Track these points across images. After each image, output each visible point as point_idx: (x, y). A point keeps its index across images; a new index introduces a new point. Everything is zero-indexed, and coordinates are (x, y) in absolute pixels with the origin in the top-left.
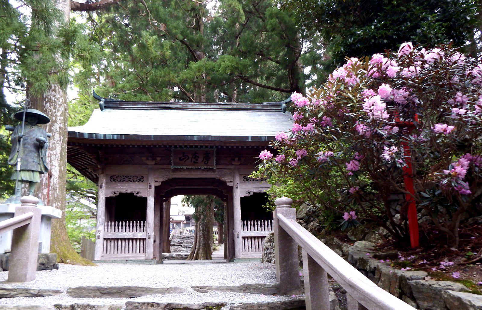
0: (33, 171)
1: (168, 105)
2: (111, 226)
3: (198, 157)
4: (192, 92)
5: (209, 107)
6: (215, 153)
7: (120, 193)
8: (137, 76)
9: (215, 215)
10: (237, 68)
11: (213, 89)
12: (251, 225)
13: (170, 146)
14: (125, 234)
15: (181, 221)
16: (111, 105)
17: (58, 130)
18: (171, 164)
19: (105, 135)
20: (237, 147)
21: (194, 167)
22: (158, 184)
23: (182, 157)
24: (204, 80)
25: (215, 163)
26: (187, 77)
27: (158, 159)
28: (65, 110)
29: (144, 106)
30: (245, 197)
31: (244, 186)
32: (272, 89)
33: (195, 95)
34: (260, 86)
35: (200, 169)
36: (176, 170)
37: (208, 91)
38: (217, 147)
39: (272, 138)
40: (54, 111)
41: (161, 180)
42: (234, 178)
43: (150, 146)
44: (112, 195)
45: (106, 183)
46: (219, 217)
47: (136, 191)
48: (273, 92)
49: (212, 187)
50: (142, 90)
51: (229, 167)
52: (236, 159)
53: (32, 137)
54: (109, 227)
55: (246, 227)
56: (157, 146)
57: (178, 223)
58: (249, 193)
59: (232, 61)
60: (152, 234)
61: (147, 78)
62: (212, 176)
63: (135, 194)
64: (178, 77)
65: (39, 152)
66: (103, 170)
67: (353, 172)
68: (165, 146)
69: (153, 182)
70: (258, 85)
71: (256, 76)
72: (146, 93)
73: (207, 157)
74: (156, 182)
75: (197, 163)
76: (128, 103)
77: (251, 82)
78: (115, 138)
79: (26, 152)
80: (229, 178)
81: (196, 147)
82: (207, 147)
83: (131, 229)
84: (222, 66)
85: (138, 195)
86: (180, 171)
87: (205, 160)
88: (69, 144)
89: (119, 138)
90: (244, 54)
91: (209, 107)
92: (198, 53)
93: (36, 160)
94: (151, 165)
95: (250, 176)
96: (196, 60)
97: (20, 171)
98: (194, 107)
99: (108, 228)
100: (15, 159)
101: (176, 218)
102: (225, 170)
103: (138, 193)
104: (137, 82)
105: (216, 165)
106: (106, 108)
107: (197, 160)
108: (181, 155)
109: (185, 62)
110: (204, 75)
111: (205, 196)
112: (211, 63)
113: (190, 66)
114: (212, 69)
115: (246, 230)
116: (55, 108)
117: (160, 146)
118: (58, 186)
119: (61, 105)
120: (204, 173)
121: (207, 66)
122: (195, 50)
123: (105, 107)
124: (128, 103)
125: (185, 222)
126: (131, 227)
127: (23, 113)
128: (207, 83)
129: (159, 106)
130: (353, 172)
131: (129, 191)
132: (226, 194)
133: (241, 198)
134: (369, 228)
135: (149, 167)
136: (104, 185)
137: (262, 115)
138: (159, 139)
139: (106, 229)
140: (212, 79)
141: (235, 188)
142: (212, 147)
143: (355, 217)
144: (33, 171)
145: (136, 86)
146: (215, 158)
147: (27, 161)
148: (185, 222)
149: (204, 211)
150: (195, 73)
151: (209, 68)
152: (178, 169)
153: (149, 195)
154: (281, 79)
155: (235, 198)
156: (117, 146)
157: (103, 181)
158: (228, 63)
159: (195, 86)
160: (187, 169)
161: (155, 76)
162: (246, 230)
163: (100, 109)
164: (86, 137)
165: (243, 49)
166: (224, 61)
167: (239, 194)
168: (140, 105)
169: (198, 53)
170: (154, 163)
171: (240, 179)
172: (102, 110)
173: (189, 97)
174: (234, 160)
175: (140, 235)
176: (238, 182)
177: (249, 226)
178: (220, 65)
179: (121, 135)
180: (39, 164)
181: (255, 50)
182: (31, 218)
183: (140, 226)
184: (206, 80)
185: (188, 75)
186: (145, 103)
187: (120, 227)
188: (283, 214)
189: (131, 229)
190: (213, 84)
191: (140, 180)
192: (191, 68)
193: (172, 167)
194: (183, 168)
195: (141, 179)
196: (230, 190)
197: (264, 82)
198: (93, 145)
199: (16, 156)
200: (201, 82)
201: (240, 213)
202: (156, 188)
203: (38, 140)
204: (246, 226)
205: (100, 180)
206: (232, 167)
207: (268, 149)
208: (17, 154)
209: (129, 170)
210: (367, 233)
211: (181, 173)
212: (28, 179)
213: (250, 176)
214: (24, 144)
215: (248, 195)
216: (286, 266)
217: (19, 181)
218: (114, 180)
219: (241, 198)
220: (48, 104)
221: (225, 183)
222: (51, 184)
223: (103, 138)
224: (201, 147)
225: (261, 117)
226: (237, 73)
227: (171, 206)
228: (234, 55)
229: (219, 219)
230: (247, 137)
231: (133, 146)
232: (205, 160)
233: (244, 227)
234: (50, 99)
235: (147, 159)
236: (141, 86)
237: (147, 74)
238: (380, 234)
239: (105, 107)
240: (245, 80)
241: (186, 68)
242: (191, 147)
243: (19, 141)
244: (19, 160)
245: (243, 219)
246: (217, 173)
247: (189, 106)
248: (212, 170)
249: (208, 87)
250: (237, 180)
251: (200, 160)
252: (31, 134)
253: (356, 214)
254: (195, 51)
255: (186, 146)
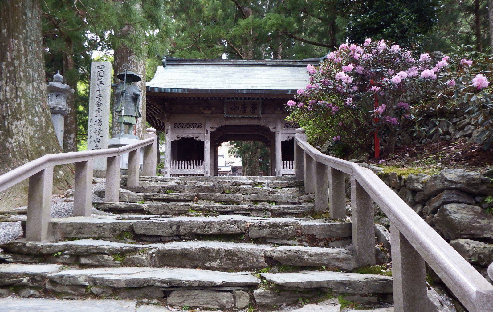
0: (132, 116)
1: (221, 62)
2: (176, 164)
3: (247, 107)
4: (240, 47)
5: (256, 63)
6: (260, 104)
7: (182, 138)
8: (190, 34)
9: (261, 163)
10: (281, 26)
11: (260, 44)
12: (290, 164)
13: (224, 98)
14: (187, 170)
15: (227, 172)
16: (172, 63)
17: (140, 86)
18: (224, 114)
19: (171, 89)
20: (279, 99)
21: (243, 116)
22: (213, 130)
23: (234, 108)
24: (251, 37)
25: (260, 113)
26: (236, 34)
27: (214, 109)
28: (144, 69)
29: (200, 63)
30: (286, 141)
31: (284, 132)
32: (315, 44)
33: (243, 49)
34: (305, 42)
35: (248, 117)
36: (228, 118)
37: (255, 46)
38: (262, 98)
39: (295, 92)
40: (136, 70)
41: (216, 127)
42: (276, 125)
43: (208, 98)
44: (176, 139)
45: (171, 129)
46: (264, 166)
47: (196, 135)
48: (316, 47)
49: (257, 133)
50: (195, 47)
51: (272, 116)
52: (279, 109)
53: (130, 92)
54: (174, 165)
55: (285, 167)
56: (213, 98)
57: (225, 173)
58: (289, 138)
59: (278, 19)
60: (209, 171)
61: (200, 36)
62: (258, 124)
63: (195, 138)
64: (227, 34)
65: (135, 103)
66: (169, 118)
67: (336, 112)
68: (220, 98)
69: (210, 128)
70: (302, 40)
71: (300, 31)
72: (198, 50)
73: (254, 107)
74: (212, 128)
75: (246, 112)
76: (185, 60)
77: (295, 38)
78: (180, 92)
79: (127, 103)
80: (272, 126)
81: (245, 98)
82: (254, 99)
83: (192, 167)
84: (269, 23)
85: (198, 139)
86: (232, 119)
87: (252, 110)
88: (147, 97)
89: (183, 92)
90: (288, 12)
91: (256, 63)
92: (246, 9)
93: (133, 108)
94: (207, 114)
95: (285, 120)
96: (244, 17)
97: (125, 116)
98: (243, 63)
99: (173, 166)
100: (120, 107)
101: (223, 169)
102: (269, 119)
103: (197, 138)
104: (191, 40)
105: (262, 114)
106: (168, 65)
107: (246, 110)
108: (233, 106)
109: (233, 17)
110: (251, 31)
111: (252, 142)
112: (258, 21)
113: (238, 23)
114: (259, 27)
115: (285, 169)
116: (137, 69)
117: (216, 98)
118: (141, 129)
119: (141, 66)
120: (252, 121)
121: (254, 23)
122: (243, 6)
123: (167, 64)
124: (185, 60)
125: (231, 173)
126: (192, 165)
127: (124, 74)
128: (254, 39)
129: (213, 63)
130: (336, 112)
131: (190, 136)
132: (268, 139)
133: (282, 142)
134: (360, 152)
135: (206, 115)
136: (169, 131)
137: (302, 70)
138: (214, 92)
139: (172, 167)
140: (259, 35)
141: (277, 133)
142: (258, 99)
143: (339, 139)
144: (132, 116)
145: (191, 44)
146: (261, 108)
147: (128, 109)
148: (231, 173)
149: (250, 156)
150: (243, 30)
151: (256, 25)
152: (230, 117)
153: (206, 139)
154: (323, 35)
155: (277, 142)
156: (181, 98)
157: (168, 127)
158: (274, 21)
159: (242, 42)
160: (237, 117)
161: (207, 33)
162: (285, 169)
163: (162, 66)
164: (157, 90)
165: (288, 6)
166: (270, 19)
167: (280, 139)
168: (196, 63)
169: (246, 9)
170: (209, 112)
171: (282, 127)
172: (164, 67)
173: (238, 55)
174: (277, 110)
175: (199, 171)
176: (280, 128)
177: (288, 165)
178: (266, 22)
179: (185, 89)
180: (136, 111)
181: (299, 8)
182: (153, 140)
183: (199, 164)
184: (253, 37)
185: (237, 32)
186: (201, 61)
187: (183, 165)
188: (299, 138)
189: (192, 167)
190: (260, 40)
191: (198, 127)
192: (240, 25)
193: (225, 116)
194: (233, 117)
195: (199, 126)
196: (273, 136)
197: (307, 38)
198: (162, 98)
199: (120, 105)
200: (248, 38)
201: (281, 155)
202: (212, 133)
203: (135, 94)
204: (285, 165)
205: (166, 127)
206: (275, 116)
207: (293, 99)
208: (121, 104)
209: (188, 118)
210: (359, 156)
211: (233, 121)
212: (129, 122)
213: (285, 120)
214: (126, 97)
215: (288, 140)
216: (300, 167)
217: (123, 123)
218: (177, 127)
219: (282, 142)
220: (132, 66)
221: (269, 129)
222: (137, 127)
223: (169, 92)
224: (249, 98)
225: (301, 72)
226: (282, 30)
227: (219, 158)
228: (279, 13)
229: (264, 168)
230: (287, 90)
231: (194, 98)
232: (252, 110)
233: (284, 166)
234: (133, 61)
235: (205, 109)
236: (194, 43)
237: (200, 31)
238: (366, 156)
239: (167, 64)
240: (289, 36)
241: (234, 25)
242: (241, 98)
243: (122, 95)
244: (123, 108)
245: (283, 159)
246: (262, 121)
247: (239, 63)
248: (258, 118)
249: (255, 43)
250: (279, 127)
251: (248, 109)
252: (130, 89)
253: (340, 137)
254: (243, 7)
255: (237, 98)
